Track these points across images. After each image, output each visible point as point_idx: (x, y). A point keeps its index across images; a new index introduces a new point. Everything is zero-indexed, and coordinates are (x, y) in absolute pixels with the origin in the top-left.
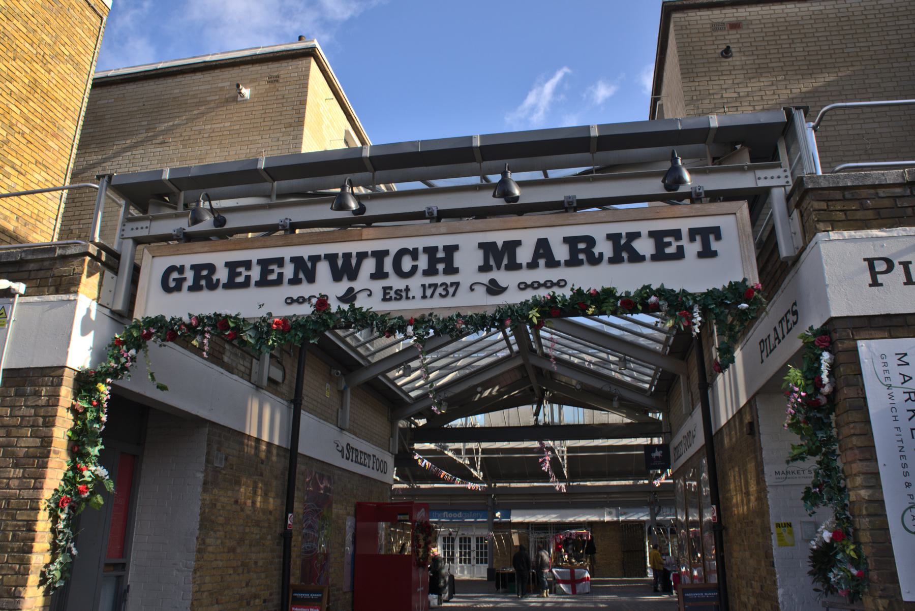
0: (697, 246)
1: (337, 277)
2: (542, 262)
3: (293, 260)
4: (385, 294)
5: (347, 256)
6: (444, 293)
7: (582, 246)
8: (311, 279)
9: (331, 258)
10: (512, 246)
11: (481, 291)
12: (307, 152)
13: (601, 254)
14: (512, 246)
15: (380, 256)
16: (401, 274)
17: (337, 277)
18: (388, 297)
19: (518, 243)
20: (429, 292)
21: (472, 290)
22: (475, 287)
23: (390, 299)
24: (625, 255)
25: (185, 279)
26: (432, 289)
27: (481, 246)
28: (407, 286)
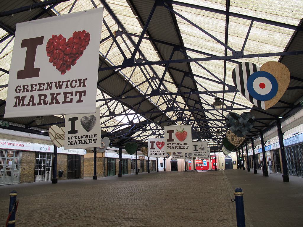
0: (77, 98)
8: (51, 89)
12: (137, 38)
19: (26, 97)
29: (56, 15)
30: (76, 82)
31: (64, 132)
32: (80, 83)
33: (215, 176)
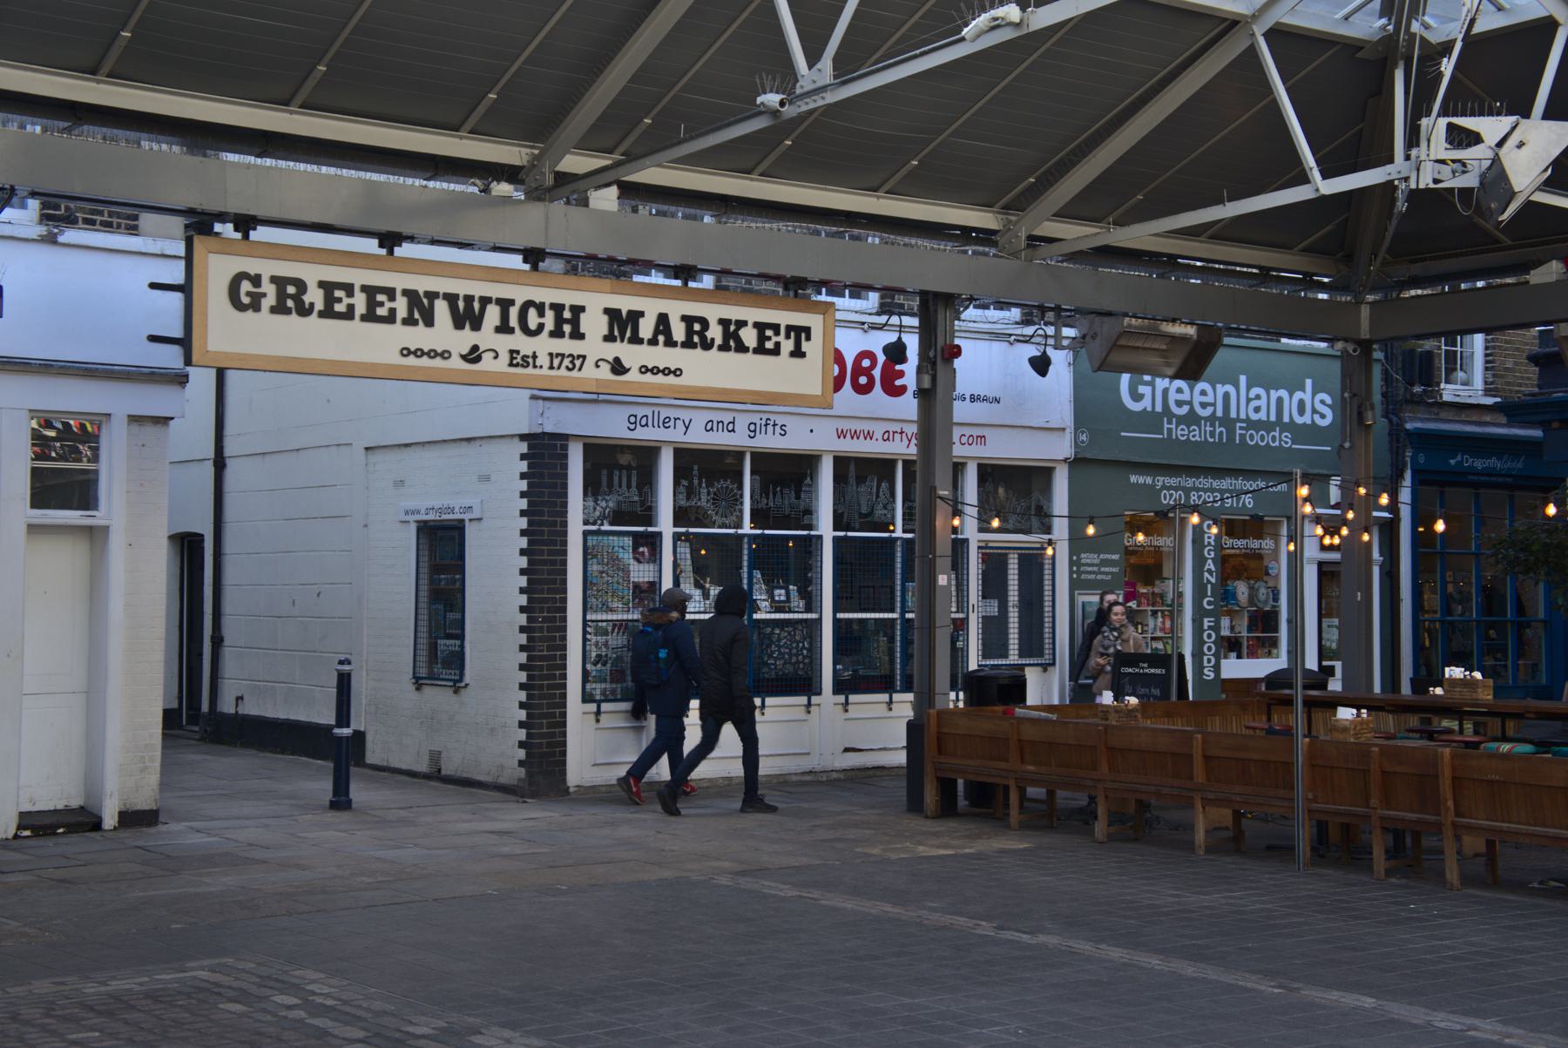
1: (459, 324)
2: (661, 338)
3: (406, 293)
4: (512, 358)
5: (469, 299)
6: (570, 366)
7: (291, 290)
9: (451, 299)
10: (635, 316)
11: (605, 367)
13: (312, 305)
14: (635, 316)
15: (505, 304)
16: (527, 331)
17: (459, 324)
18: (515, 362)
19: (641, 314)
20: (556, 362)
21: (598, 366)
22: (599, 364)
23: (517, 365)
24: (732, 343)
25: (264, 295)
26: (581, 359)
27: (607, 311)
28: (535, 353)
29: (1053, 216)
30: (541, 314)
31: (349, 549)
32: (559, 321)
33: (860, 506)
